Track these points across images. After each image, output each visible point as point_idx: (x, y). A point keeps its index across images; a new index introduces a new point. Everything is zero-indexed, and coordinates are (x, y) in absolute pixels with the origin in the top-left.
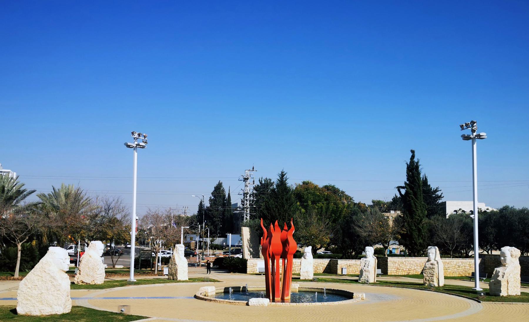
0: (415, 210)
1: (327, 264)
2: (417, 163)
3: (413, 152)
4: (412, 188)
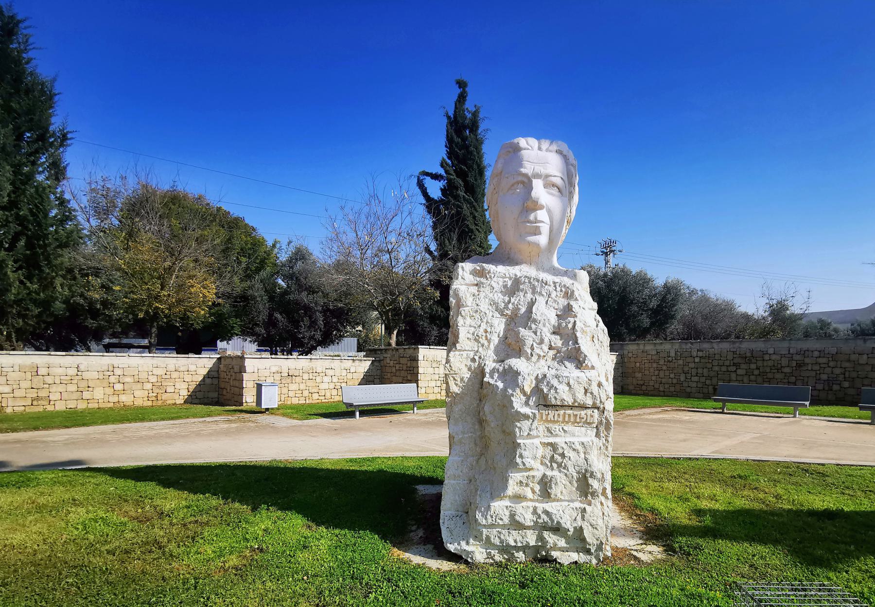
0: (473, 227)
1: (204, 372)
2: (475, 114)
3: (462, 84)
4: (461, 174)
